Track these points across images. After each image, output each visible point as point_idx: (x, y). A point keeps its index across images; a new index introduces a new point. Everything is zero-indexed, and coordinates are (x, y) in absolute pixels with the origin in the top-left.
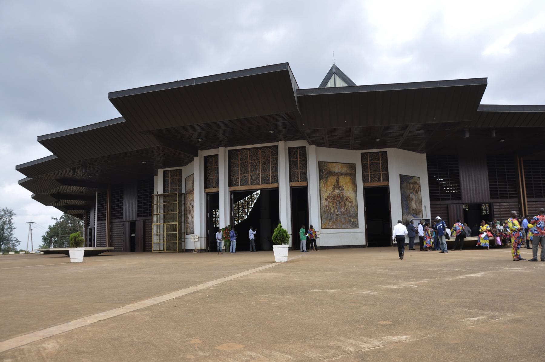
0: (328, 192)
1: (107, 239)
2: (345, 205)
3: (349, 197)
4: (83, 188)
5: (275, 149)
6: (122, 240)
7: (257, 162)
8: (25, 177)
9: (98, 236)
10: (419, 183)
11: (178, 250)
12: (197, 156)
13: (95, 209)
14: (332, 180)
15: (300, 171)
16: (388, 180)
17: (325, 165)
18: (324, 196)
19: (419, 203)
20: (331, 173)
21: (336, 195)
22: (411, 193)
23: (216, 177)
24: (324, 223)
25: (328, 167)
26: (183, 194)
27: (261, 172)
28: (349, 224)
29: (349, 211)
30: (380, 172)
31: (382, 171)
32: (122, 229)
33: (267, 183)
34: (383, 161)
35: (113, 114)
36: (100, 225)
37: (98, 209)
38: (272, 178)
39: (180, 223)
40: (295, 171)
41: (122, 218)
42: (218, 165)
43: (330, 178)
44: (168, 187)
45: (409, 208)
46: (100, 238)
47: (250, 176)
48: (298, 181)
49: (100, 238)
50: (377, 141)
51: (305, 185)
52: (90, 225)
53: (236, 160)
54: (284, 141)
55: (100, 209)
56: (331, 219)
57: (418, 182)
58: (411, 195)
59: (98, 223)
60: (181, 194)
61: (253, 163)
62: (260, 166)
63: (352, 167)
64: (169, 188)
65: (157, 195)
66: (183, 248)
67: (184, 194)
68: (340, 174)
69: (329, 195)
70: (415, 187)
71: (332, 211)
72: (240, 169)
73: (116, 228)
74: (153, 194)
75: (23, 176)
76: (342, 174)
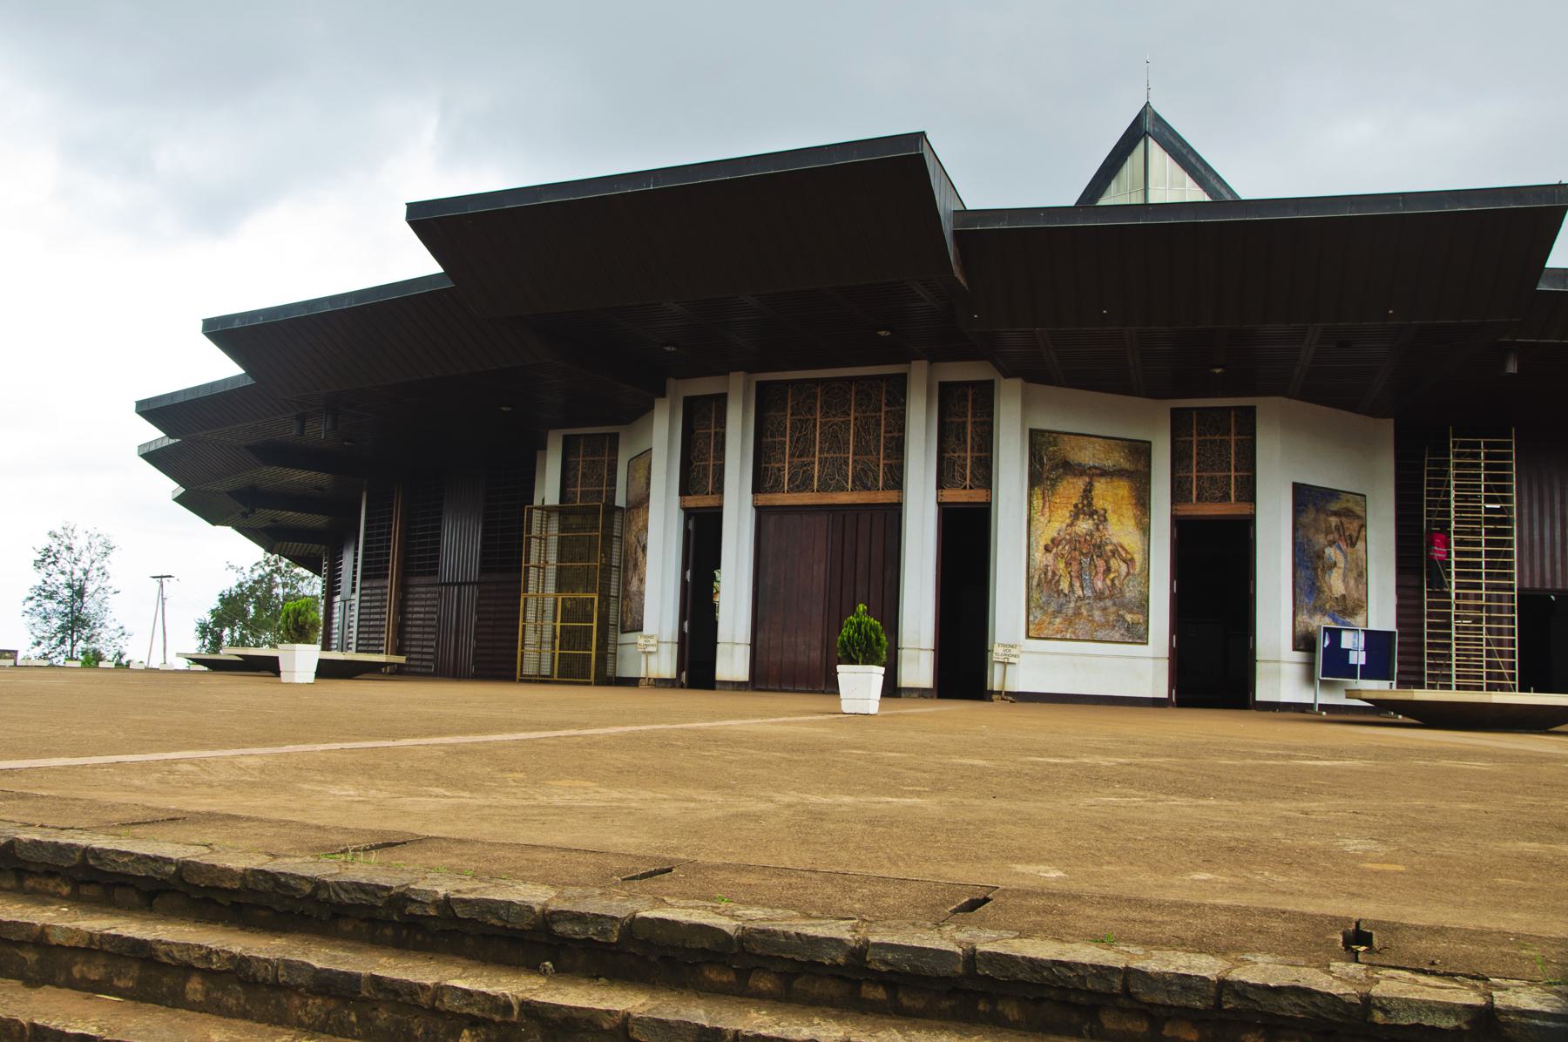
0: (1055, 524)
1: (390, 607)
2: (1108, 570)
4: (326, 476)
6: (432, 640)
7: (843, 422)
8: (161, 434)
9: (363, 626)
10: (1362, 514)
11: (592, 679)
12: (663, 395)
13: (357, 543)
14: (1071, 489)
15: (972, 457)
16: (1251, 498)
17: (1050, 442)
19: (1356, 580)
21: (1080, 536)
22: (1331, 543)
23: (716, 462)
24: (1037, 621)
25: (1060, 449)
27: (854, 454)
28: (1117, 628)
29: (1121, 589)
30: (1229, 470)
31: (1236, 470)
32: (434, 606)
33: (869, 489)
34: (1239, 437)
35: (418, 262)
36: (369, 591)
37: (366, 543)
38: (884, 472)
39: (605, 598)
40: (956, 455)
41: (435, 573)
42: (724, 427)
43: (1065, 483)
44: (576, 486)
45: (1320, 591)
46: (371, 601)
47: (820, 463)
48: (965, 488)
49: (371, 601)
50: (1215, 373)
51: (984, 500)
52: (339, 593)
53: (782, 414)
54: (926, 362)
55: (371, 542)
56: (1059, 612)
57: (1358, 510)
58: (1331, 552)
59: (362, 586)
60: (611, 509)
61: (829, 425)
62: (849, 434)
63: (1141, 451)
64: (579, 489)
65: (542, 508)
66: (609, 673)
67: (622, 508)
68: (1098, 472)
69: (1056, 535)
70: (1345, 526)
71: (1064, 586)
72: (791, 441)
73: (415, 603)
74: (532, 504)
75: (152, 434)
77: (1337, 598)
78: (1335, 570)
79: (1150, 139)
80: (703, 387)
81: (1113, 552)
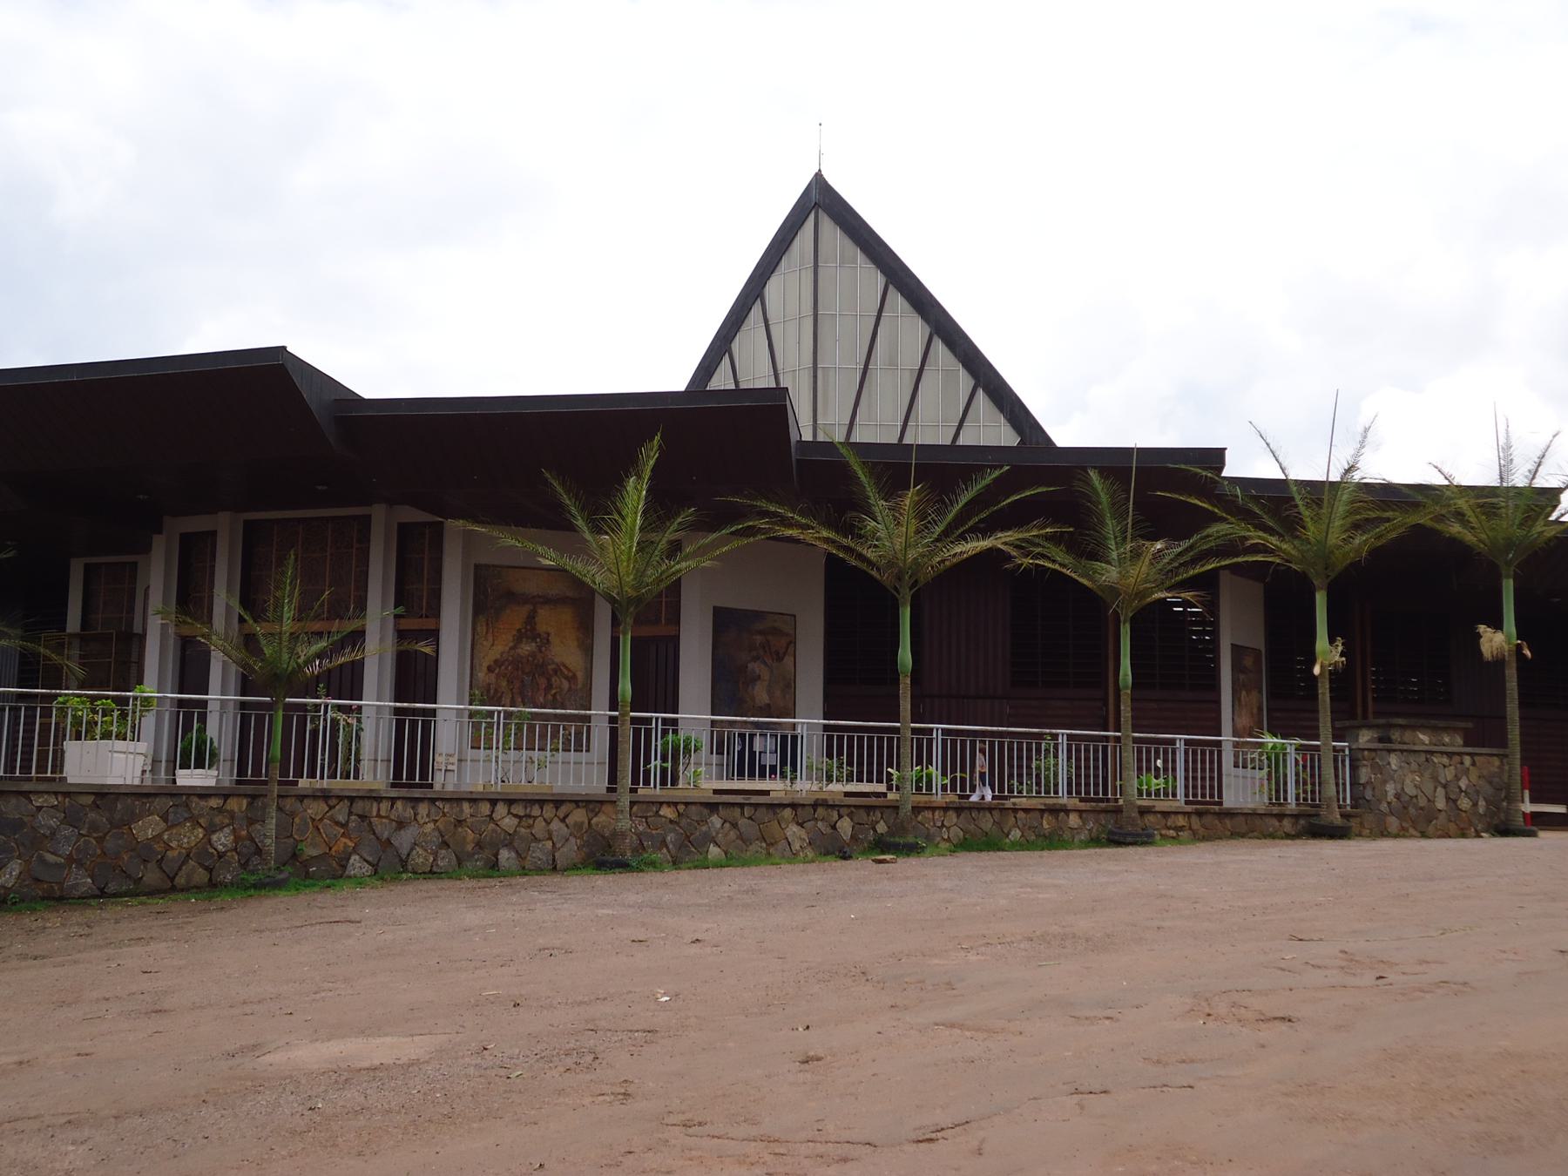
0: (496, 649)
2: (549, 687)
3: (564, 666)
5: (366, 522)
10: (792, 632)
12: (160, 532)
14: (515, 617)
18: (484, 658)
20: (511, 597)
21: (522, 657)
22: (755, 659)
26: (137, 634)
48: (421, 617)
51: (434, 628)
58: (755, 667)
64: (100, 616)
68: (541, 600)
69: (499, 656)
76: (547, 601)
77: (761, 708)
78: (758, 683)
79: (820, 210)
80: (197, 524)
81: (555, 671)
